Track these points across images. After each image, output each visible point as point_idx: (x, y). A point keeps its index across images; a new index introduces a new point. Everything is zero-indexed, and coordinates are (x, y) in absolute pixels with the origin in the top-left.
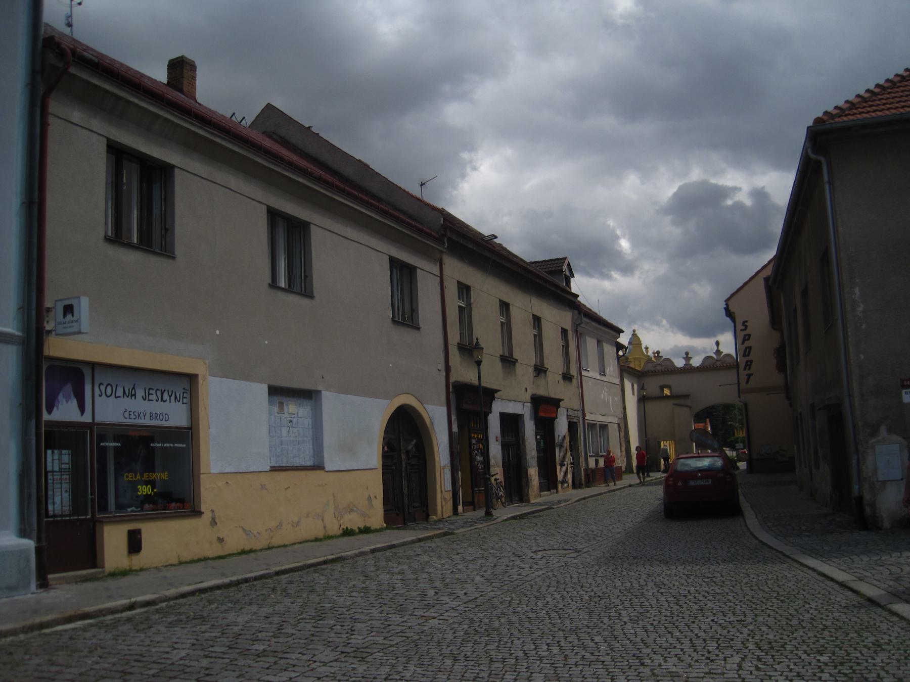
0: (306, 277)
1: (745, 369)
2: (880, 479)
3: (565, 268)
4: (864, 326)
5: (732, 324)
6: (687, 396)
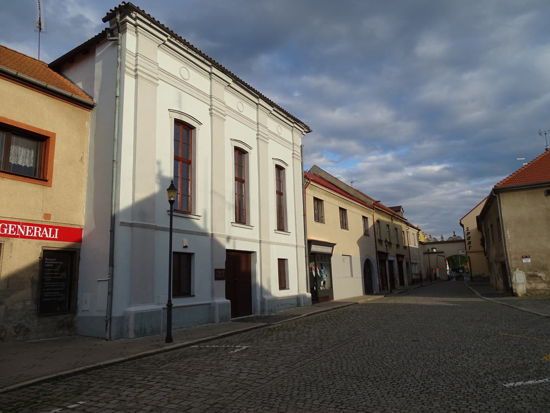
1: (468, 245)
3: (401, 210)
4: (510, 241)
6: (443, 252)
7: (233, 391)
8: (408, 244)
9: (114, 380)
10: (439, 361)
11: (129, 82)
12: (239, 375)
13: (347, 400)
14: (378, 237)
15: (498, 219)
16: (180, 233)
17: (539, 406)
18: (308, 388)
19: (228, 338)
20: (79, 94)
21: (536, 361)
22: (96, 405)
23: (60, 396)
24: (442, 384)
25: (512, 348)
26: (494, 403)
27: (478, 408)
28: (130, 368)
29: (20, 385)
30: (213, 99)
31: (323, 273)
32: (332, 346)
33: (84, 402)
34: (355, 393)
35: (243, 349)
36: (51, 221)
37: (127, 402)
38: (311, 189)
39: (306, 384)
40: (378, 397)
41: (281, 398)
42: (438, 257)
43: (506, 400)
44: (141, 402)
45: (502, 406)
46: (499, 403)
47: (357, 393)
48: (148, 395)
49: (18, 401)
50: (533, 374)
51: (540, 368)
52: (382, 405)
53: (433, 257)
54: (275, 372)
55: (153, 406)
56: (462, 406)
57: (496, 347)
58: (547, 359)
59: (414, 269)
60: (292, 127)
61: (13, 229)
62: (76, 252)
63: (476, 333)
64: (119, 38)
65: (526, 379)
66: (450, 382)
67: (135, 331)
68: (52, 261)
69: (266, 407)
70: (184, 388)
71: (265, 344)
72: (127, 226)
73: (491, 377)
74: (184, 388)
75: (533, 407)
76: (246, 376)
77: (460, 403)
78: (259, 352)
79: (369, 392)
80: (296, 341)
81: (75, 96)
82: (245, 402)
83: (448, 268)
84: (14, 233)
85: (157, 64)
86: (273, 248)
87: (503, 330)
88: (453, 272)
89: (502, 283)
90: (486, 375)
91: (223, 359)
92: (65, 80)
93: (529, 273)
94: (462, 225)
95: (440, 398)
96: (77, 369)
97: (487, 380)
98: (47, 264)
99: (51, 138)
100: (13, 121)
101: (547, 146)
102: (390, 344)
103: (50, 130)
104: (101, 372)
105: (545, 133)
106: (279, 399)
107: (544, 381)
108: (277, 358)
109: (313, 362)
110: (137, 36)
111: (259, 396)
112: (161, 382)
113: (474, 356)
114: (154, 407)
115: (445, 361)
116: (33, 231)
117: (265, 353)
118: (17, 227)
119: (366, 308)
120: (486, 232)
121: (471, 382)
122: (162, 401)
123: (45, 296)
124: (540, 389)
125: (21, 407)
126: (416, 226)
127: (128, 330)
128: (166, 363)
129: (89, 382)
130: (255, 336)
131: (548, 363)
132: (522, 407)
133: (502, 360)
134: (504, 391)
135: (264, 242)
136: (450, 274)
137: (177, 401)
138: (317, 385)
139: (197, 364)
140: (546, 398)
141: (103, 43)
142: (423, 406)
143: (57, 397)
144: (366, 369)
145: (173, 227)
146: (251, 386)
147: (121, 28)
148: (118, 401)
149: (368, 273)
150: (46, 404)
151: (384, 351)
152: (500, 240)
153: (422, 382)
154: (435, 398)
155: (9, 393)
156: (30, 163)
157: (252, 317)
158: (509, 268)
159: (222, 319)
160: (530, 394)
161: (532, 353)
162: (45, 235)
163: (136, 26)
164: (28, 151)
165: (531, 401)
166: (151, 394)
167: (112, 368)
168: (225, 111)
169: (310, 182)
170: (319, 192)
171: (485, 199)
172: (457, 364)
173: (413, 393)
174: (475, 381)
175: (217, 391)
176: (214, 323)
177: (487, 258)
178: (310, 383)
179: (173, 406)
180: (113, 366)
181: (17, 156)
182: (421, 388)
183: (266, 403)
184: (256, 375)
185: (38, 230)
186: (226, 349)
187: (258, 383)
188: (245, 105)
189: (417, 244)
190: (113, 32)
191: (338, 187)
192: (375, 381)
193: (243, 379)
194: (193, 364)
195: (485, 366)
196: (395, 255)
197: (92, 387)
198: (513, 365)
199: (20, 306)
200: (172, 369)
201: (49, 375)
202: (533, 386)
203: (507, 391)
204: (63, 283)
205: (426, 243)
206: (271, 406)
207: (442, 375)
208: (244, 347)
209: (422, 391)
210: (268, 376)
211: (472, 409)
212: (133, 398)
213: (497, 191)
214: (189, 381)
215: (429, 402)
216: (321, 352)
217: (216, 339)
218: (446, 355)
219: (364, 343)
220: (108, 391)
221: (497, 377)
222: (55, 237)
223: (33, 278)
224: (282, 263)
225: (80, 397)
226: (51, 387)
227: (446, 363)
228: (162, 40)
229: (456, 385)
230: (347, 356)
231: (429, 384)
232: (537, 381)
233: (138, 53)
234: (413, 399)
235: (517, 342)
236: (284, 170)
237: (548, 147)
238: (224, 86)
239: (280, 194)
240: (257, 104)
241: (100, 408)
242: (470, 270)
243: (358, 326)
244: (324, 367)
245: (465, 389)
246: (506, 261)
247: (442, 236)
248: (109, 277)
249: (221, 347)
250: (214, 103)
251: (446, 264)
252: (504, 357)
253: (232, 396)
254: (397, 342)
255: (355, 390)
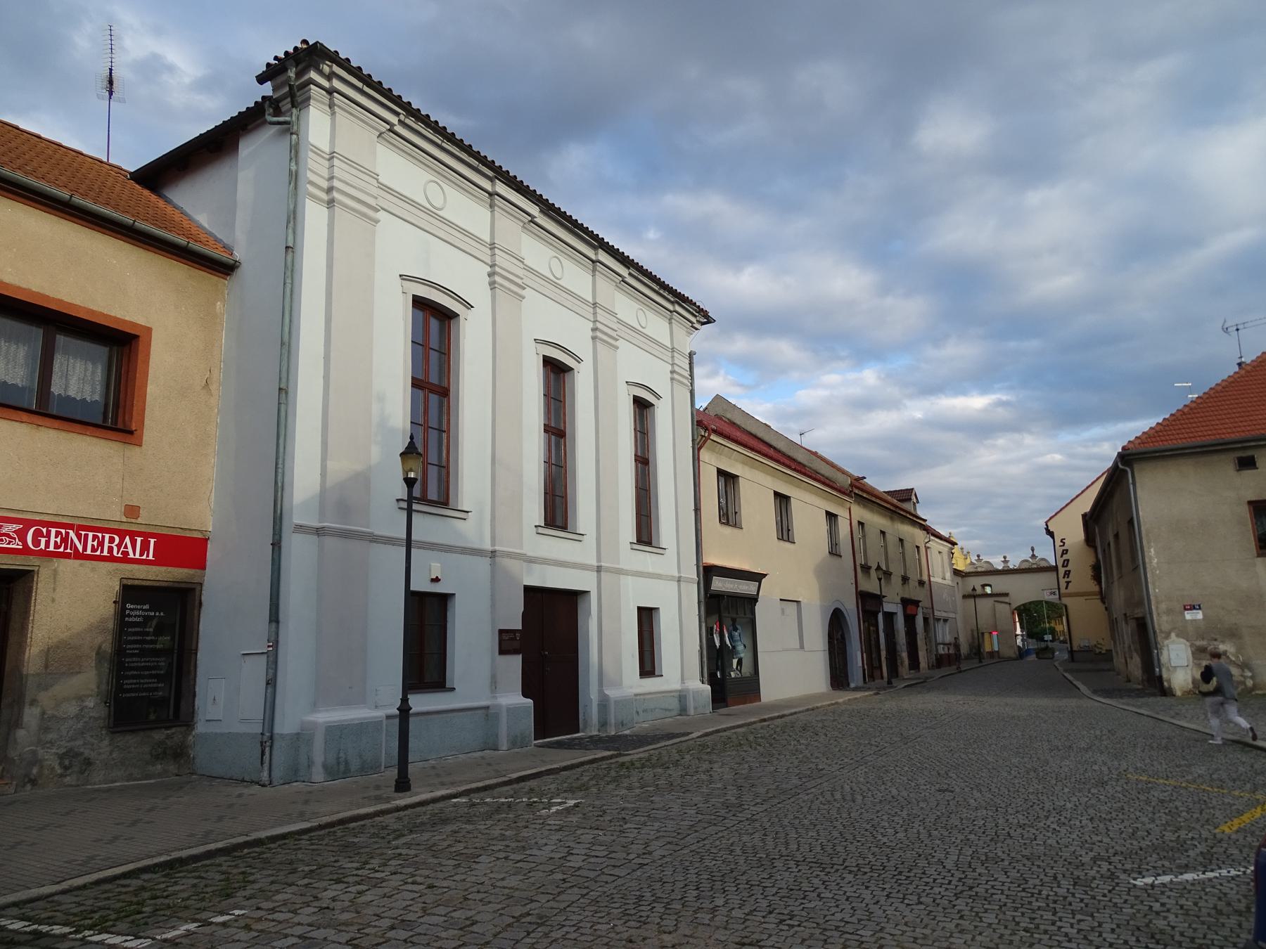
0: (789, 530)
1: (1064, 577)
2: (1173, 665)
3: (913, 497)
4: (1158, 572)
5: (1052, 540)
6: (1006, 595)
7: (559, 890)
8: (929, 576)
9: (296, 869)
10: (996, 833)
11: (314, 216)
12: (568, 858)
13: (802, 910)
14: (860, 560)
15: (1131, 522)
16: (424, 548)
17: (1203, 923)
18: (718, 885)
19: (533, 783)
20: (203, 239)
21: (1205, 834)
22: (270, 917)
23: (188, 899)
24: (1003, 878)
25: (1154, 808)
26: (1110, 917)
27: (1075, 926)
28: (326, 845)
29: (95, 877)
30: (497, 251)
31: (737, 641)
32: (764, 800)
33: (243, 912)
34: (818, 896)
35: (568, 805)
36: (139, 520)
37: (337, 912)
38: (712, 450)
39: (714, 878)
40: (867, 905)
41: (663, 905)
42: (997, 604)
43: (1135, 911)
44: (365, 911)
45: (1126, 923)
46: (1121, 917)
47: (822, 895)
48: (377, 898)
49: (100, 908)
50: (1196, 860)
51: (1212, 848)
52: (876, 919)
53: (985, 605)
54: (644, 854)
55: (393, 919)
56: (1043, 922)
57: (1119, 805)
58: (1227, 831)
59: (940, 632)
60: (671, 312)
61: (58, 540)
62: (194, 590)
63: (1077, 776)
64: (294, 118)
65: (1180, 871)
66: (1019, 875)
67: (325, 766)
68: (140, 610)
69: (633, 923)
70: (452, 885)
71: (617, 796)
72: (308, 533)
73: (1105, 866)
74: (452, 885)
75: (1190, 925)
76: (583, 861)
77: (1038, 916)
78: (605, 812)
79: (848, 894)
80: (683, 790)
81: (195, 246)
82: (586, 913)
83: (1019, 631)
84: (60, 547)
85: (375, 176)
86: (628, 581)
87: (1137, 768)
88: (1030, 640)
89: (1140, 665)
90: (1095, 863)
91: (527, 827)
92: (169, 209)
93: (1200, 643)
94: (1050, 533)
95: (998, 907)
96: (212, 846)
97: (1098, 872)
98: (129, 616)
99: (141, 339)
100: (60, 301)
101: (1241, 357)
102: (890, 796)
103: (141, 321)
104: (264, 853)
105: (1235, 328)
106: (659, 908)
107: (1218, 875)
108: (644, 824)
109: (725, 833)
110: (333, 114)
111: (615, 900)
112: (401, 873)
113: (1072, 822)
114: (396, 922)
115: (1008, 833)
116: (101, 544)
117: (618, 813)
118: (67, 534)
119: (834, 720)
120: (1104, 551)
121: (1064, 876)
122: (410, 911)
123: (125, 687)
124: (1207, 890)
125: (111, 920)
126: (944, 533)
127: (310, 765)
128: (404, 835)
129: (243, 873)
130: (591, 779)
131: (1229, 838)
132: (1169, 925)
133: (1131, 830)
134: (1131, 893)
135: (609, 570)
136: (1024, 645)
137: (442, 910)
138: (736, 880)
139: (471, 835)
140: (1219, 908)
141: (257, 127)
142: (961, 922)
143: (182, 901)
144: (839, 848)
145: (413, 538)
146: (596, 882)
147: (296, 98)
148: (317, 910)
149: (837, 640)
150: (164, 915)
151: (878, 812)
152: (1136, 568)
153: (958, 875)
154: (985, 906)
155: (75, 893)
156: (93, 392)
157: (580, 738)
158: (1155, 632)
159: (515, 742)
160: (1187, 900)
161: (1197, 818)
162: (127, 553)
163: (330, 92)
164: (90, 366)
165: (1187, 914)
166: (385, 896)
167: (285, 844)
168: (522, 279)
169: (709, 435)
170: (730, 458)
171: (1103, 474)
172: (1035, 840)
173: (940, 896)
174: (1072, 874)
175: (525, 890)
176: (496, 749)
177: (1106, 609)
178: (722, 876)
179: (435, 920)
180: (287, 841)
181: (66, 377)
182: (957, 886)
183: (631, 915)
184: (604, 859)
185: (112, 540)
186: (530, 805)
187: (611, 875)
188: (567, 263)
189: (948, 575)
190: (280, 105)
191: (770, 446)
192: (859, 873)
193: (577, 866)
194: (463, 836)
195: (1094, 844)
196: (898, 600)
197: (253, 882)
198: (1155, 841)
199: (72, 709)
200: (418, 847)
201: (153, 857)
202: (1193, 884)
203: (1138, 894)
204: (163, 659)
205: (969, 573)
206: (643, 919)
207: (1003, 860)
208: (571, 803)
209: (960, 893)
210: (630, 862)
211: (1062, 927)
212: (347, 904)
213: (1129, 459)
214: (461, 870)
215: (973, 914)
216: (740, 812)
217: (506, 785)
218: (1011, 820)
219: (832, 795)
220: (289, 890)
221: (1119, 866)
222: (148, 556)
223: (100, 647)
224: (647, 616)
225: (231, 901)
226: (163, 883)
227: (1011, 837)
228: (388, 124)
229: (1031, 882)
230: (797, 822)
231: (975, 879)
232: (1204, 873)
233: (334, 152)
234: (940, 909)
235: (1166, 794)
236: (651, 408)
237: (1243, 360)
238: (522, 221)
239: (644, 461)
240: (593, 262)
241: (280, 922)
242: (1068, 637)
243: (817, 758)
244: (749, 845)
245: (1049, 889)
246: (1148, 616)
247: (1005, 557)
248: (269, 646)
249: (519, 802)
250: (498, 260)
251: (1015, 622)
252: (1135, 825)
253: (557, 901)
254: (905, 794)
255: (817, 890)
